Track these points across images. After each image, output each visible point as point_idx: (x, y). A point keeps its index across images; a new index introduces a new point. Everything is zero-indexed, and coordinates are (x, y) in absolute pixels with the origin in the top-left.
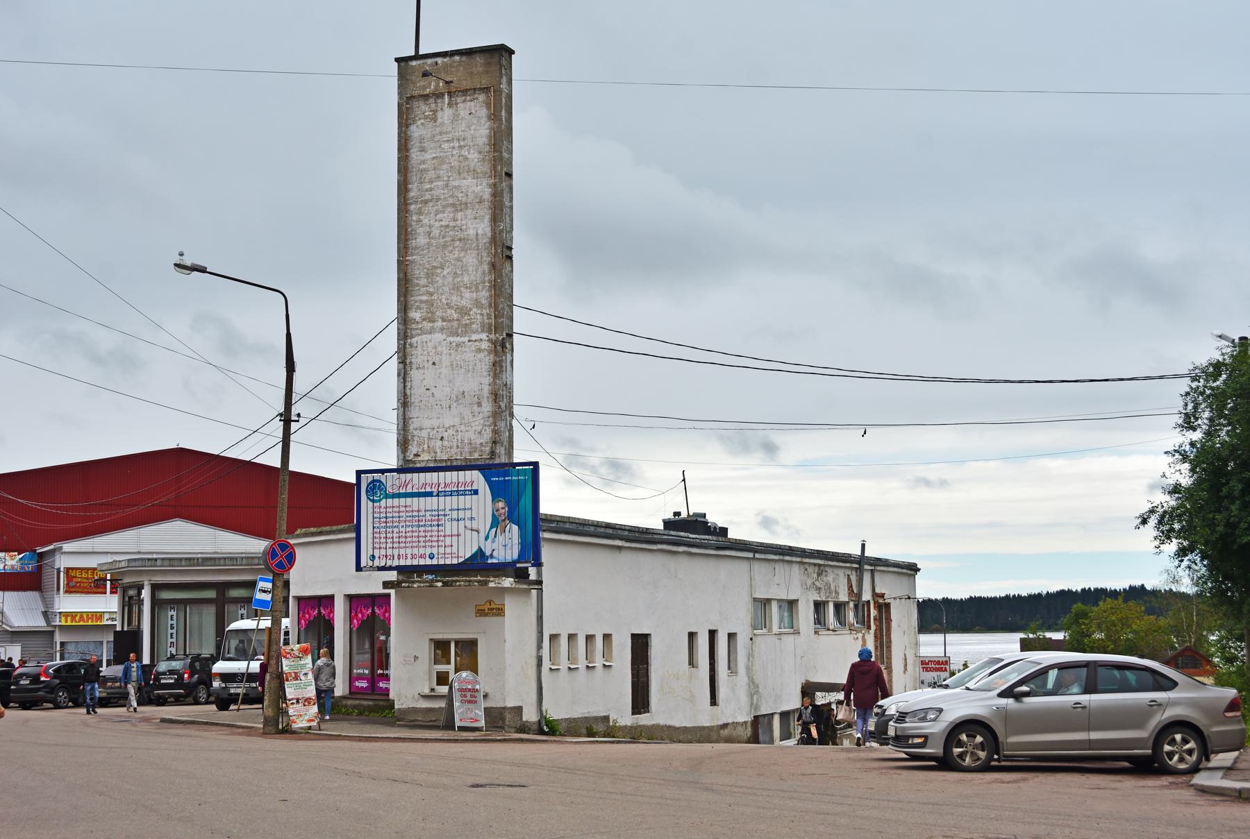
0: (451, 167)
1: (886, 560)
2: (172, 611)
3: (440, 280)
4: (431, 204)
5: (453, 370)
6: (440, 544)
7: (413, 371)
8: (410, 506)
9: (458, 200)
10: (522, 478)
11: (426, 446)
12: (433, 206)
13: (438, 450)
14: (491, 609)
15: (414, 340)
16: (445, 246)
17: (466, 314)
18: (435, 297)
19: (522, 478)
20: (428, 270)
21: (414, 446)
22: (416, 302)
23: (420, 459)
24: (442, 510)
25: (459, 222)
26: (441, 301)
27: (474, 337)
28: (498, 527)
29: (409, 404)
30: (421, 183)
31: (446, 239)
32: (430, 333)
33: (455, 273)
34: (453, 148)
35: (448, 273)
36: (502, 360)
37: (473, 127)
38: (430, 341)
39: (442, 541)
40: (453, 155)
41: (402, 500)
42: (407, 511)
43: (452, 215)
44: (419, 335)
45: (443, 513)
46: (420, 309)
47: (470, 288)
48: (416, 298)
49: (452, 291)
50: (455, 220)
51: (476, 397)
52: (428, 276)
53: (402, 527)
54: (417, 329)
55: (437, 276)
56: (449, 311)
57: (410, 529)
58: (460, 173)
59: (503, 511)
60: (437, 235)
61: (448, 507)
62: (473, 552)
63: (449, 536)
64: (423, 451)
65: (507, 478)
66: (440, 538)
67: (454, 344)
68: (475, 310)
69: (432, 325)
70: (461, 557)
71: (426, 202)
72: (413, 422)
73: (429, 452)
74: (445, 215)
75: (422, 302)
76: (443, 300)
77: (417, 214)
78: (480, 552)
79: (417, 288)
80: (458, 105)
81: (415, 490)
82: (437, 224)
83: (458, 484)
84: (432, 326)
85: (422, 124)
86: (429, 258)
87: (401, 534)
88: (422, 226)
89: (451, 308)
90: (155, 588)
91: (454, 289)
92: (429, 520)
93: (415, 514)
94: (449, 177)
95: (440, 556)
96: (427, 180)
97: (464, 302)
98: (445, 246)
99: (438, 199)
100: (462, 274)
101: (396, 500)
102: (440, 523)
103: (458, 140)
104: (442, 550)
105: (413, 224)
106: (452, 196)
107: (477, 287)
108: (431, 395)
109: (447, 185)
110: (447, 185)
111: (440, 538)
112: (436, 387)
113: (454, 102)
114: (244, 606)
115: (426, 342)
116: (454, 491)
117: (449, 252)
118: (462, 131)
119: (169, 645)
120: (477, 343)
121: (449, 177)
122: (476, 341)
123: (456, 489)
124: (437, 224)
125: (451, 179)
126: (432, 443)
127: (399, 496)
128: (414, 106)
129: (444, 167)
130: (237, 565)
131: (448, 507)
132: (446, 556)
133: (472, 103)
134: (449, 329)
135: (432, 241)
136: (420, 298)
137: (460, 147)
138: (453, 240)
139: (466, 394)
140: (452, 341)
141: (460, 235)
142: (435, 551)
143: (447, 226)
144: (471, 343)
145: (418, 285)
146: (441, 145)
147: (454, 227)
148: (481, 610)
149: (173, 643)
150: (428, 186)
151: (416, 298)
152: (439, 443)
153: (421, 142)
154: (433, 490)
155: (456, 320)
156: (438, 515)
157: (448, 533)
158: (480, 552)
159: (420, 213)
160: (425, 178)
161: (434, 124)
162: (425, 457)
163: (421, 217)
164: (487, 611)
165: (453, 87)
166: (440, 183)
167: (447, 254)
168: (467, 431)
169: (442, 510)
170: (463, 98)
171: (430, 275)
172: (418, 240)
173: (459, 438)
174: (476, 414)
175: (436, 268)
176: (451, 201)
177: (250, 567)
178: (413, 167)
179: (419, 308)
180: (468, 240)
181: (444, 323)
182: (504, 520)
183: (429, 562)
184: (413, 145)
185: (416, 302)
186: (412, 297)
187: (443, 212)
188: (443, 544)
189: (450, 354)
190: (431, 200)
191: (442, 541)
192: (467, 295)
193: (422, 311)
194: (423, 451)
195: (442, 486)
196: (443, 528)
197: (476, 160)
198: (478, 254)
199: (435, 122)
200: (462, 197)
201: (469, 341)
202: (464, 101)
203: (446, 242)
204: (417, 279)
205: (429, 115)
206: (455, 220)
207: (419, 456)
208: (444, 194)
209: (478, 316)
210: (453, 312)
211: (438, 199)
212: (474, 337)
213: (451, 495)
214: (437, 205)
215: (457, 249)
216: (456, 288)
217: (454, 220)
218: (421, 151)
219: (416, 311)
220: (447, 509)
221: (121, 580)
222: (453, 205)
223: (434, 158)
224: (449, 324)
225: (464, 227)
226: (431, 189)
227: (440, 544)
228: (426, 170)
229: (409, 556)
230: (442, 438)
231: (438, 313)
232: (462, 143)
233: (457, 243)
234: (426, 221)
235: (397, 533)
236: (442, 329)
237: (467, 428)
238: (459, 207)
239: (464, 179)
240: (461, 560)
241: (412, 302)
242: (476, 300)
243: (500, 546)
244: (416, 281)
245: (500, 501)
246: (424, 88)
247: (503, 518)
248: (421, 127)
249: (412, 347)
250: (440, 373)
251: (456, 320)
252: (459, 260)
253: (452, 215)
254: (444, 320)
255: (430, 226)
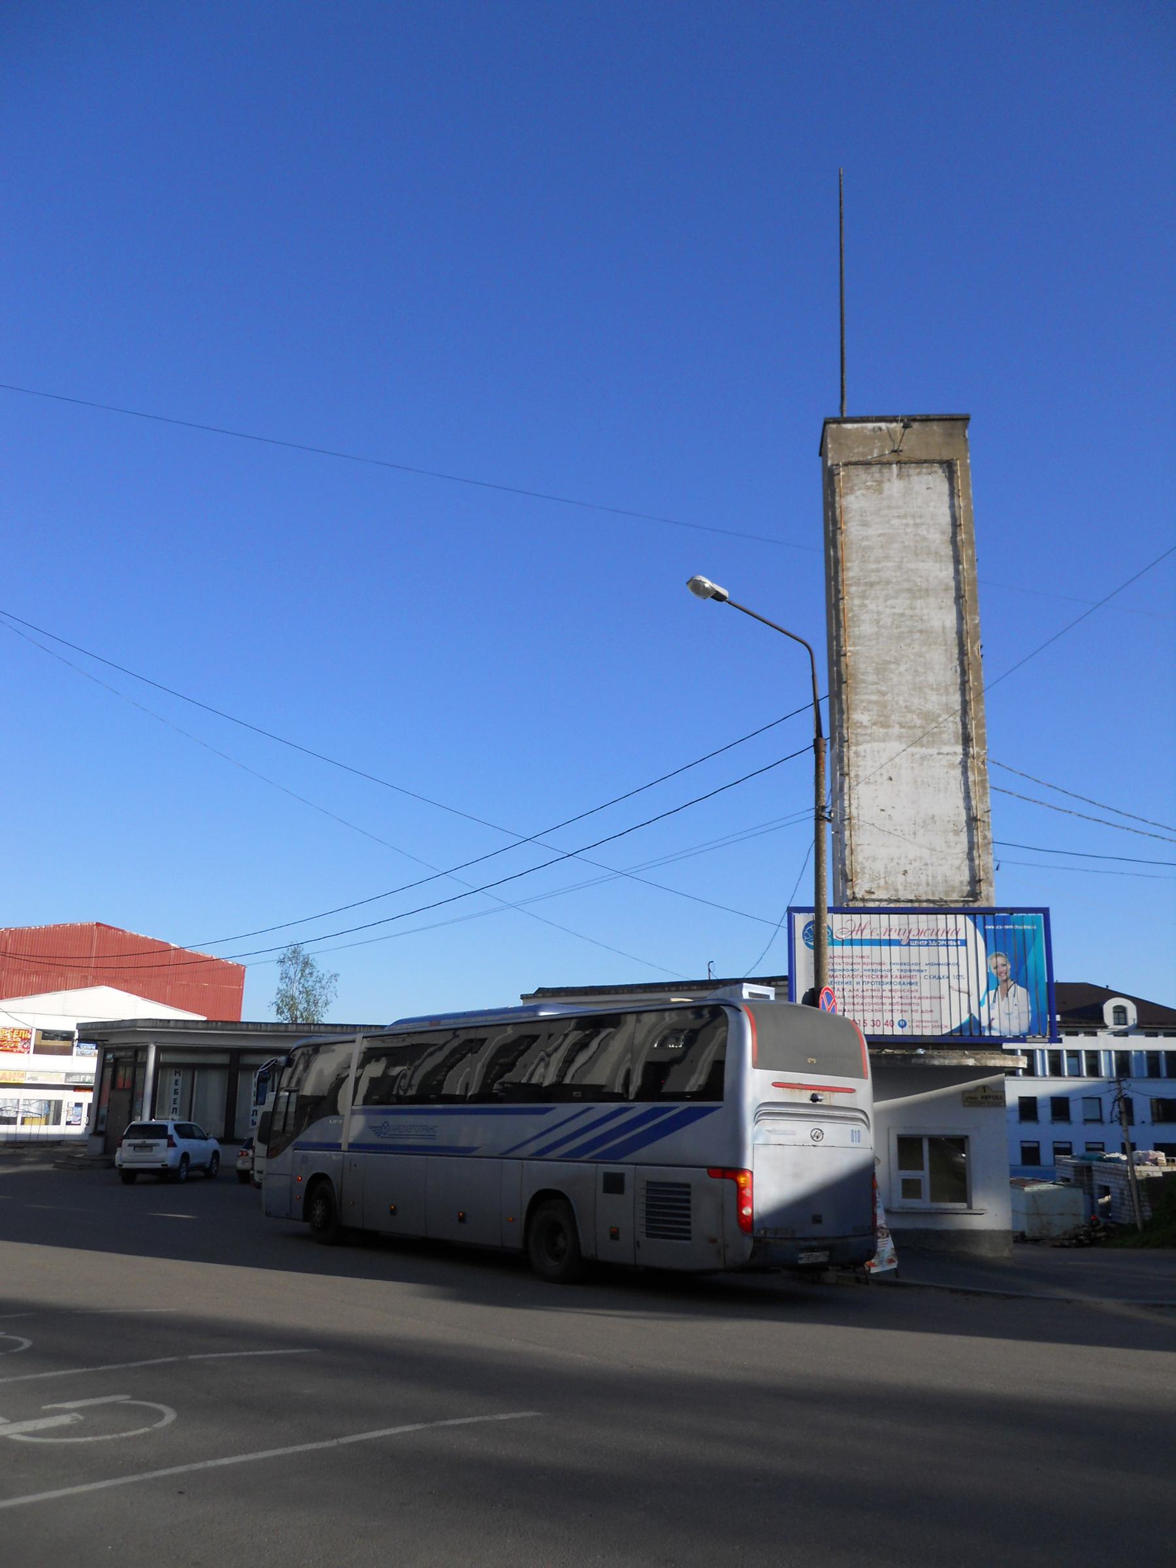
0: (905, 547)
1: (868, 417)
2: (177, 1075)
3: (895, 679)
4: (878, 587)
5: (916, 788)
6: (914, 1007)
7: (860, 786)
8: (868, 957)
9: (917, 585)
10: (1029, 927)
11: (882, 882)
12: (883, 590)
13: (900, 888)
14: (986, 1097)
15: (861, 748)
16: (900, 637)
17: (933, 720)
18: (889, 697)
19: (1029, 927)
20: (877, 664)
21: (865, 880)
22: (862, 701)
23: (873, 897)
24: (916, 964)
25: (917, 611)
26: (897, 703)
27: (945, 749)
28: (997, 989)
29: (857, 827)
30: (864, 562)
31: (902, 630)
32: (884, 741)
33: (916, 671)
34: (907, 525)
35: (906, 670)
36: (985, 780)
37: (932, 504)
38: (884, 750)
39: (918, 1004)
40: (906, 534)
41: (857, 949)
42: (863, 964)
43: (908, 602)
44: (868, 742)
45: (917, 968)
46: (869, 711)
47: (937, 690)
48: (863, 697)
49: (913, 692)
50: (912, 608)
51: (951, 823)
52: (877, 671)
53: (858, 983)
54: (865, 735)
55: (891, 672)
56: (909, 716)
57: (869, 987)
58: (917, 555)
59: (1004, 968)
60: (889, 624)
61: (925, 960)
62: (746, 977)
63: (927, 998)
64: (879, 887)
65: (1007, 927)
66: (914, 1001)
67: (918, 756)
68: (945, 716)
69: (885, 730)
70: (946, 1027)
71: (872, 585)
72: (862, 851)
73: (887, 889)
74: (898, 601)
75: (870, 702)
76: (901, 703)
77: (860, 597)
78: (974, 1023)
79: (864, 685)
80: (912, 478)
81: (875, 937)
82: (888, 611)
83: (900, 930)
84: (886, 733)
85: (863, 495)
86: (878, 650)
87: (855, 993)
88: (867, 612)
89: (911, 711)
90: (159, 1050)
91: (914, 689)
92: (896, 977)
93: (875, 967)
94: (902, 558)
95: (914, 1024)
96: (872, 558)
97: (929, 706)
98: (900, 637)
99: (888, 582)
100: (926, 673)
101: (847, 948)
102: (913, 981)
103: (913, 517)
104: (917, 1016)
105: (855, 608)
106: (908, 580)
107: (946, 688)
108: (887, 817)
109: (900, 567)
110: (900, 567)
111: (914, 1001)
112: (893, 807)
113: (906, 473)
114: (179, 1072)
115: (878, 752)
116: (932, 940)
117: (906, 645)
118: (917, 507)
119: (252, 1113)
120: (949, 757)
121: (902, 558)
122: (948, 754)
123: (934, 938)
124: (888, 611)
125: (905, 560)
126: (890, 880)
127: (852, 942)
128: (852, 474)
129: (896, 546)
130: (260, 1031)
131: (925, 960)
132: (924, 1024)
133: (930, 477)
134: (909, 737)
135: (883, 630)
136: (867, 697)
137: (916, 525)
138: (911, 632)
139: (936, 818)
140: (915, 753)
141: (920, 626)
142: (907, 1017)
143: (903, 615)
144: (941, 756)
145: (864, 681)
146: (890, 520)
147: (912, 616)
148: (971, 1098)
149: (176, 1109)
150: (874, 566)
151: (863, 697)
152: (901, 878)
153: (862, 516)
154: (902, 937)
155: (920, 727)
156: (910, 971)
157: (926, 993)
158: (974, 1023)
159: (863, 596)
160: (869, 557)
161: (880, 496)
162: (881, 894)
163: (866, 602)
164: (979, 1099)
165: (903, 457)
166: (890, 564)
167: (903, 647)
168: (940, 865)
169: (916, 964)
170: (918, 470)
171: (882, 669)
172: (861, 628)
173: (930, 873)
174: (953, 844)
175: (889, 662)
176: (906, 585)
177: (274, 1034)
178: (851, 543)
179: (866, 709)
180: (932, 632)
181: (902, 730)
182: (1006, 981)
183: (898, 1031)
184: (850, 518)
185: (862, 701)
186: (856, 695)
187: (896, 597)
188: (919, 1008)
189: (912, 768)
190: (878, 583)
191: (918, 1004)
192: (933, 697)
193: (871, 713)
194: (879, 887)
195: (915, 932)
196: (918, 988)
197: (938, 541)
198: (946, 651)
199: (881, 493)
200: (921, 582)
201: (939, 754)
202: (919, 474)
203: (902, 633)
204: (863, 674)
205: (872, 485)
206: (912, 608)
207: (873, 893)
208: (896, 577)
209: (950, 724)
210: (915, 717)
211: (888, 582)
212: (945, 749)
213: (927, 945)
214: (887, 589)
215: (917, 642)
216: (919, 689)
217: (911, 608)
218: (862, 525)
219: (862, 713)
220: (923, 963)
221: (107, 1040)
222: (909, 590)
223: (880, 535)
224: (910, 732)
225: (925, 618)
226: (878, 570)
227: (914, 1007)
228: (870, 548)
229: (870, 1023)
230: (905, 873)
231: (893, 717)
232: (918, 521)
233: (917, 636)
234: (872, 606)
235: (850, 991)
236: (900, 737)
237: (940, 862)
238: (918, 592)
239: (923, 561)
240: (946, 1031)
241: (857, 702)
242: (947, 704)
243: (1002, 1015)
244: (861, 677)
245: (999, 955)
246: (864, 454)
247: (1005, 978)
248: (861, 497)
249: (858, 756)
250: (899, 791)
251: (920, 727)
252: (920, 655)
253: (908, 602)
254: (902, 726)
255: (878, 613)
